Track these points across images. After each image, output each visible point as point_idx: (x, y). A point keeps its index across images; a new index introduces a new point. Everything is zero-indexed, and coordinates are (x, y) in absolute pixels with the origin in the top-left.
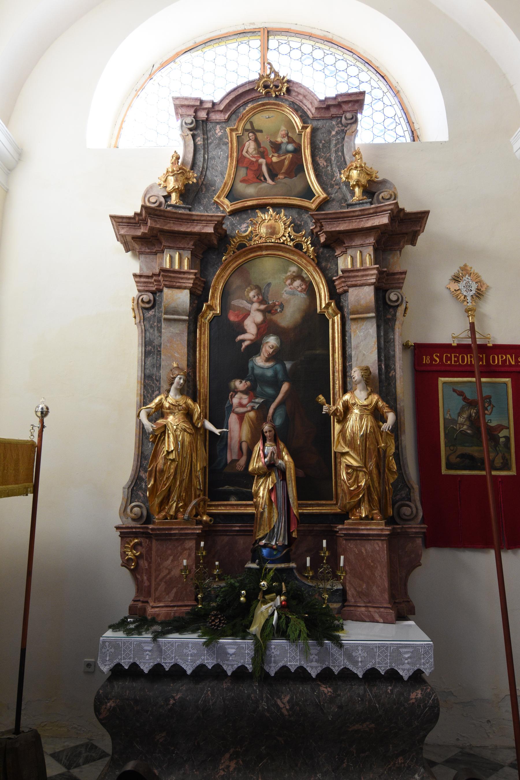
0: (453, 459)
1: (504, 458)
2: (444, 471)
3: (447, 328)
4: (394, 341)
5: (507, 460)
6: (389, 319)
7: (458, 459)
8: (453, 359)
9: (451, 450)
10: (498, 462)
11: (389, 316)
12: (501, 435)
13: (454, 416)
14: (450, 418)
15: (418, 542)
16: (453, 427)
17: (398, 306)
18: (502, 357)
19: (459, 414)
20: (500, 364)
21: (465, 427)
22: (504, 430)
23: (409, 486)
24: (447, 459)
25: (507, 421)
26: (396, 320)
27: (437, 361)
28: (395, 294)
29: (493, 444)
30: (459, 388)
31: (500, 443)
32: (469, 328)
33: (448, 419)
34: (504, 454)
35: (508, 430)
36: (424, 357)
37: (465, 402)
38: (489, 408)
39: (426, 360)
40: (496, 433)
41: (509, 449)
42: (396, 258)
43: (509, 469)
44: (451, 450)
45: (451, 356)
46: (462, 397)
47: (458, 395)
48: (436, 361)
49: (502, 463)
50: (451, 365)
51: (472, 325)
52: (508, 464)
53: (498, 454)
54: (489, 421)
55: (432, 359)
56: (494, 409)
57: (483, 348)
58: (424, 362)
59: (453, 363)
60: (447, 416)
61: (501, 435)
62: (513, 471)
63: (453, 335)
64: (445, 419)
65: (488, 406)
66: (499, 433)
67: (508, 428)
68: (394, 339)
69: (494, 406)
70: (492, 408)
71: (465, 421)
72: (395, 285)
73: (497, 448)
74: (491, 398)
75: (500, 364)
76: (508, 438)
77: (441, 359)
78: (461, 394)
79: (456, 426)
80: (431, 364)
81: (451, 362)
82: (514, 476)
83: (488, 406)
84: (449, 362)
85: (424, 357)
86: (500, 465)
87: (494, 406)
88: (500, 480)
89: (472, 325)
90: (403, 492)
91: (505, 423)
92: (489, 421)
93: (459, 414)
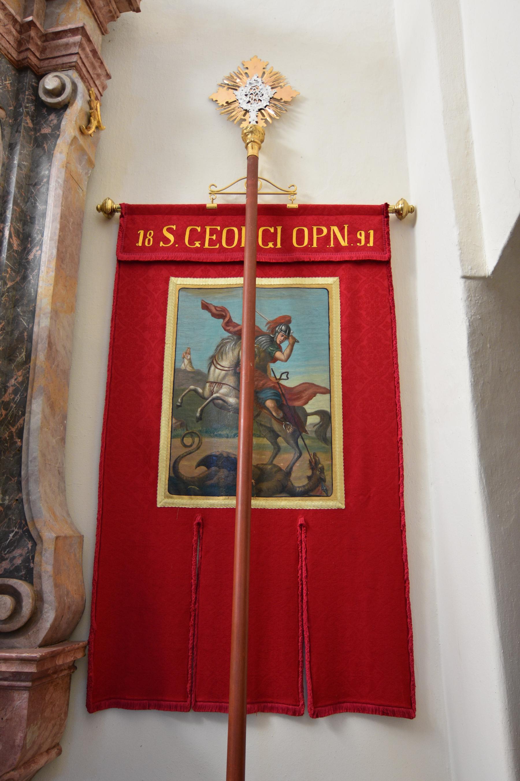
0: (190, 469)
1: (314, 465)
2: (164, 499)
3: (204, 175)
4: (48, 182)
5: (322, 470)
6: (45, 137)
7: (203, 468)
8: (208, 237)
9: (185, 446)
10: (300, 477)
11: (46, 130)
12: (309, 408)
13: (201, 365)
14: (189, 369)
15: (17, 703)
16: (195, 391)
17: (65, 106)
18: (320, 231)
19: (213, 361)
20: (315, 245)
21: (224, 390)
22: (319, 397)
23: (34, 534)
24: (174, 467)
25: (327, 375)
26: (59, 136)
27: (170, 241)
28: (57, 76)
29: (290, 430)
30: (215, 301)
31: (307, 428)
32: (245, 175)
33: (185, 371)
34: (315, 455)
35: (327, 396)
36: (142, 233)
37: (228, 331)
38: (285, 345)
39: (144, 239)
40: (297, 404)
41: (328, 441)
42: (71, 10)
43: (327, 493)
44: (185, 446)
45: (204, 231)
46: (221, 321)
47: (214, 315)
48: (167, 241)
49: (309, 478)
50: (201, 250)
51: (253, 163)
52: (324, 480)
53: (301, 454)
54: (284, 376)
55: (159, 237)
56: (296, 346)
57: (275, 214)
58: (140, 244)
59: (207, 245)
60: (184, 365)
61: (309, 408)
62: (336, 499)
63: (213, 189)
64: (176, 371)
65: (282, 342)
66: (306, 403)
67: (328, 391)
68: (49, 177)
69: (295, 341)
70: (292, 346)
71: (224, 377)
72: (60, 61)
73: (300, 442)
74: (289, 321)
75: (315, 245)
76: (326, 417)
77: (179, 236)
78: (220, 314)
79: (204, 389)
80: (155, 248)
81: (203, 244)
82: (339, 510)
83: (282, 342)
84: (197, 244)
85: (142, 233)
86: (305, 482)
87: (295, 341)
88: (301, 520)
89: (253, 163)
90: (17, 552)
91: (321, 381)
92: (284, 376)
93: (213, 361)
